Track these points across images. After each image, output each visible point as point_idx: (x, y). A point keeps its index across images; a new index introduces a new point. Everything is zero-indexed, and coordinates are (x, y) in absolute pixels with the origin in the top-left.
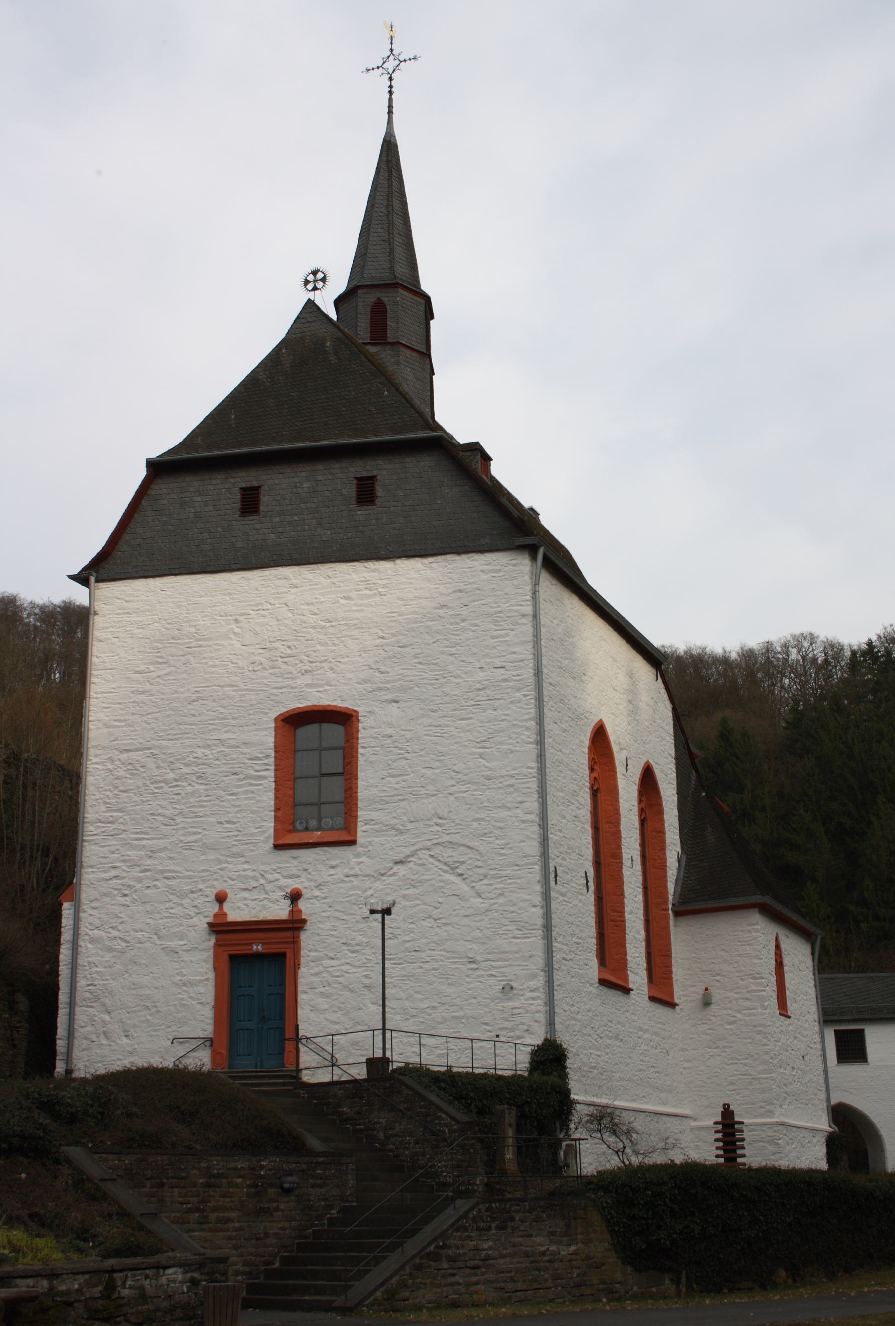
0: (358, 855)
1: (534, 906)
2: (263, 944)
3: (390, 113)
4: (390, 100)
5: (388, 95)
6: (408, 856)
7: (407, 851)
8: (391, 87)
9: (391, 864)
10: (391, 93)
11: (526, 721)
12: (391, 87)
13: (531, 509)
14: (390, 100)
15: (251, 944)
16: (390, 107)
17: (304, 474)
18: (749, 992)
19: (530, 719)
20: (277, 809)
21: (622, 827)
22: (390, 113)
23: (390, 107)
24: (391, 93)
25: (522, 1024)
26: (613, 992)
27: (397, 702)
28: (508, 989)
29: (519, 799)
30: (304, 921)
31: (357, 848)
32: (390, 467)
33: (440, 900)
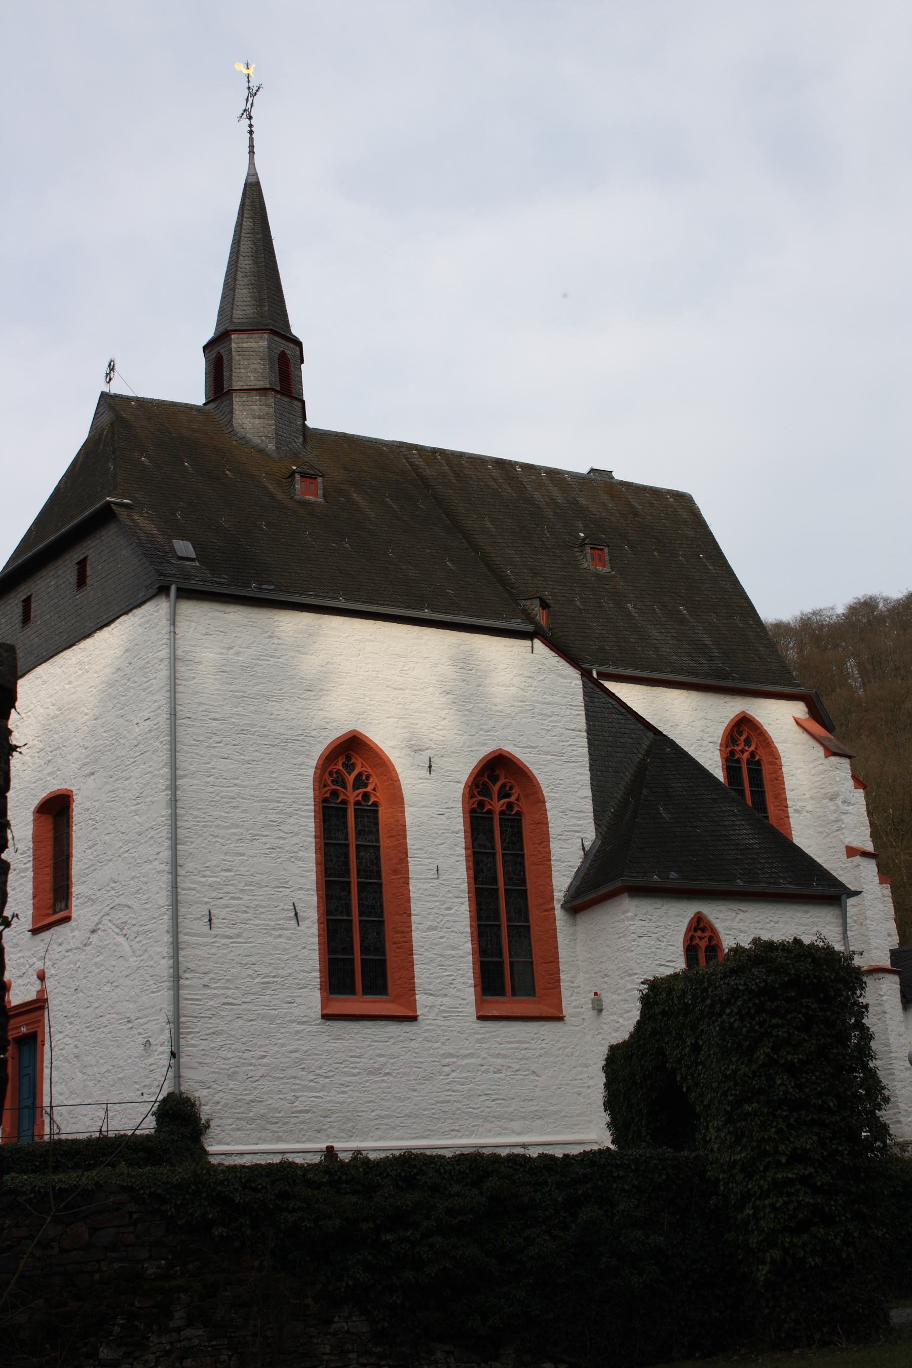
0: (73, 930)
1: (164, 958)
2: (27, 1025)
3: (252, 152)
4: (251, 140)
5: (249, 135)
6: (97, 924)
7: (96, 919)
8: (251, 126)
9: (88, 935)
10: (251, 132)
11: (161, 769)
12: (251, 126)
13: (592, 470)
14: (251, 140)
15: (20, 1027)
16: (251, 146)
17: (52, 573)
18: (627, 991)
19: (163, 767)
20: (34, 897)
21: (409, 841)
22: (252, 152)
23: (251, 146)
24: (251, 132)
25: (155, 1080)
26: (362, 1023)
27: (93, 774)
28: (147, 1044)
29: (156, 850)
30: (795, 939)
31: (72, 923)
32: (94, 544)
33: (114, 963)
